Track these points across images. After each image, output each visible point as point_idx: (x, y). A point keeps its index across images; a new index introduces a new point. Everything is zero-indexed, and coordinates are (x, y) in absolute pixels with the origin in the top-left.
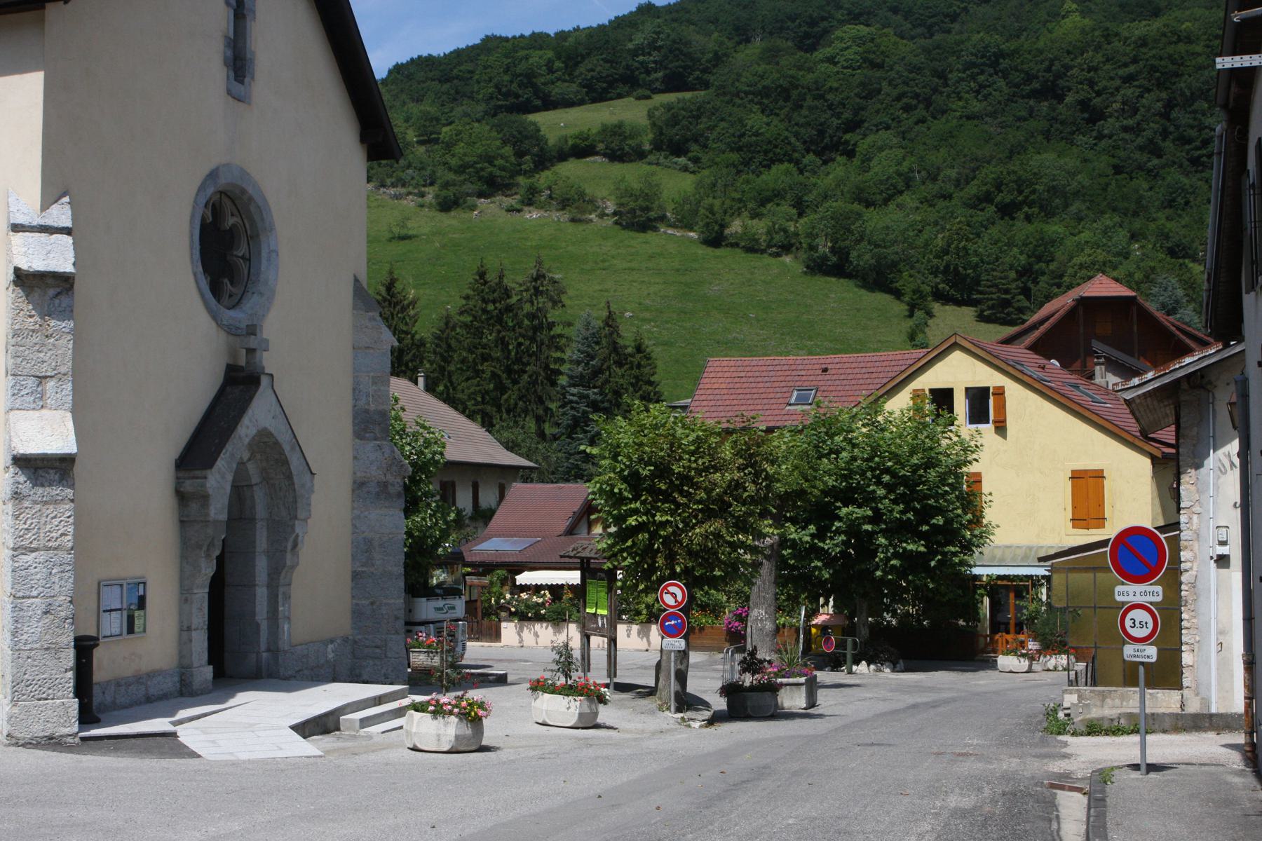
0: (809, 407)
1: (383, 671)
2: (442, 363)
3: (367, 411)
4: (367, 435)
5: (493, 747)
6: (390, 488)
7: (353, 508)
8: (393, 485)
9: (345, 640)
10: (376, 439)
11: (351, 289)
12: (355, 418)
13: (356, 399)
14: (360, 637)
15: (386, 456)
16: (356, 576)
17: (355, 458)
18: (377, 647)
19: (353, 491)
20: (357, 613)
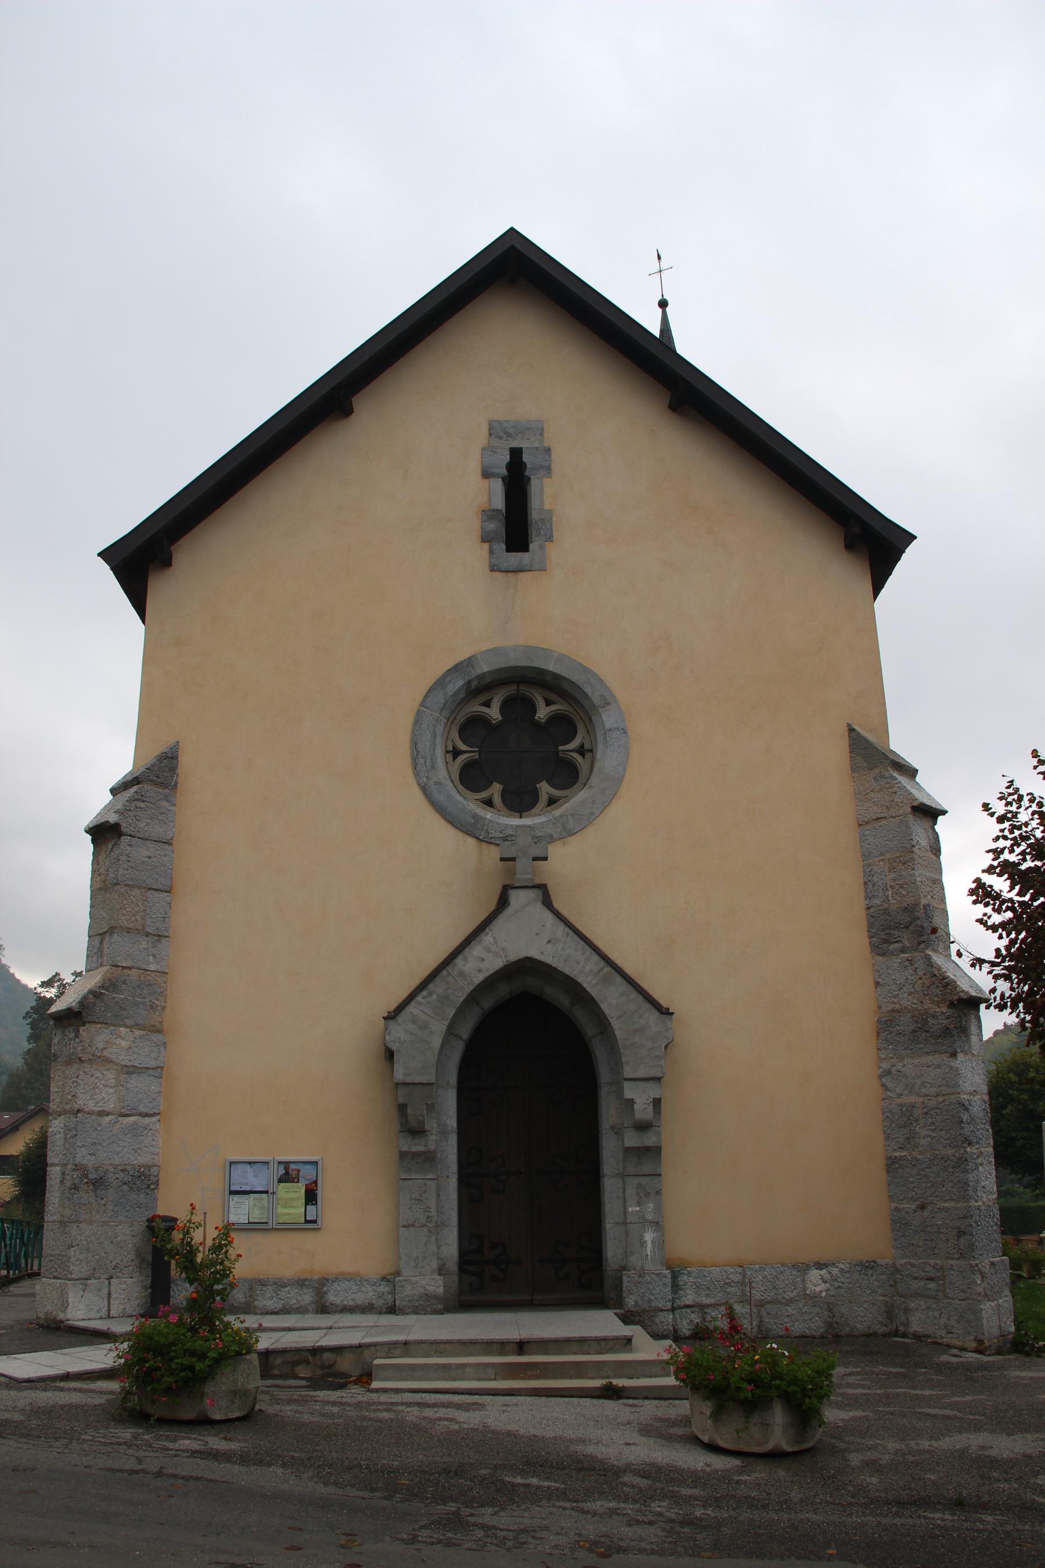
0: (917, 1410)
1: (943, 1321)
2: (990, 811)
3: (886, 912)
4: (892, 947)
5: (579, 702)
6: (931, 1021)
7: (881, 1060)
8: (934, 1016)
9: (868, 1266)
10: (903, 951)
11: (844, 744)
12: (870, 925)
13: (868, 897)
14: (903, 1262)
15: (921, 973)
16: (892, 1165)
17: (877, 984)
18: (932, 1279)
19: (878, 1034)
20: (899, 1224)
